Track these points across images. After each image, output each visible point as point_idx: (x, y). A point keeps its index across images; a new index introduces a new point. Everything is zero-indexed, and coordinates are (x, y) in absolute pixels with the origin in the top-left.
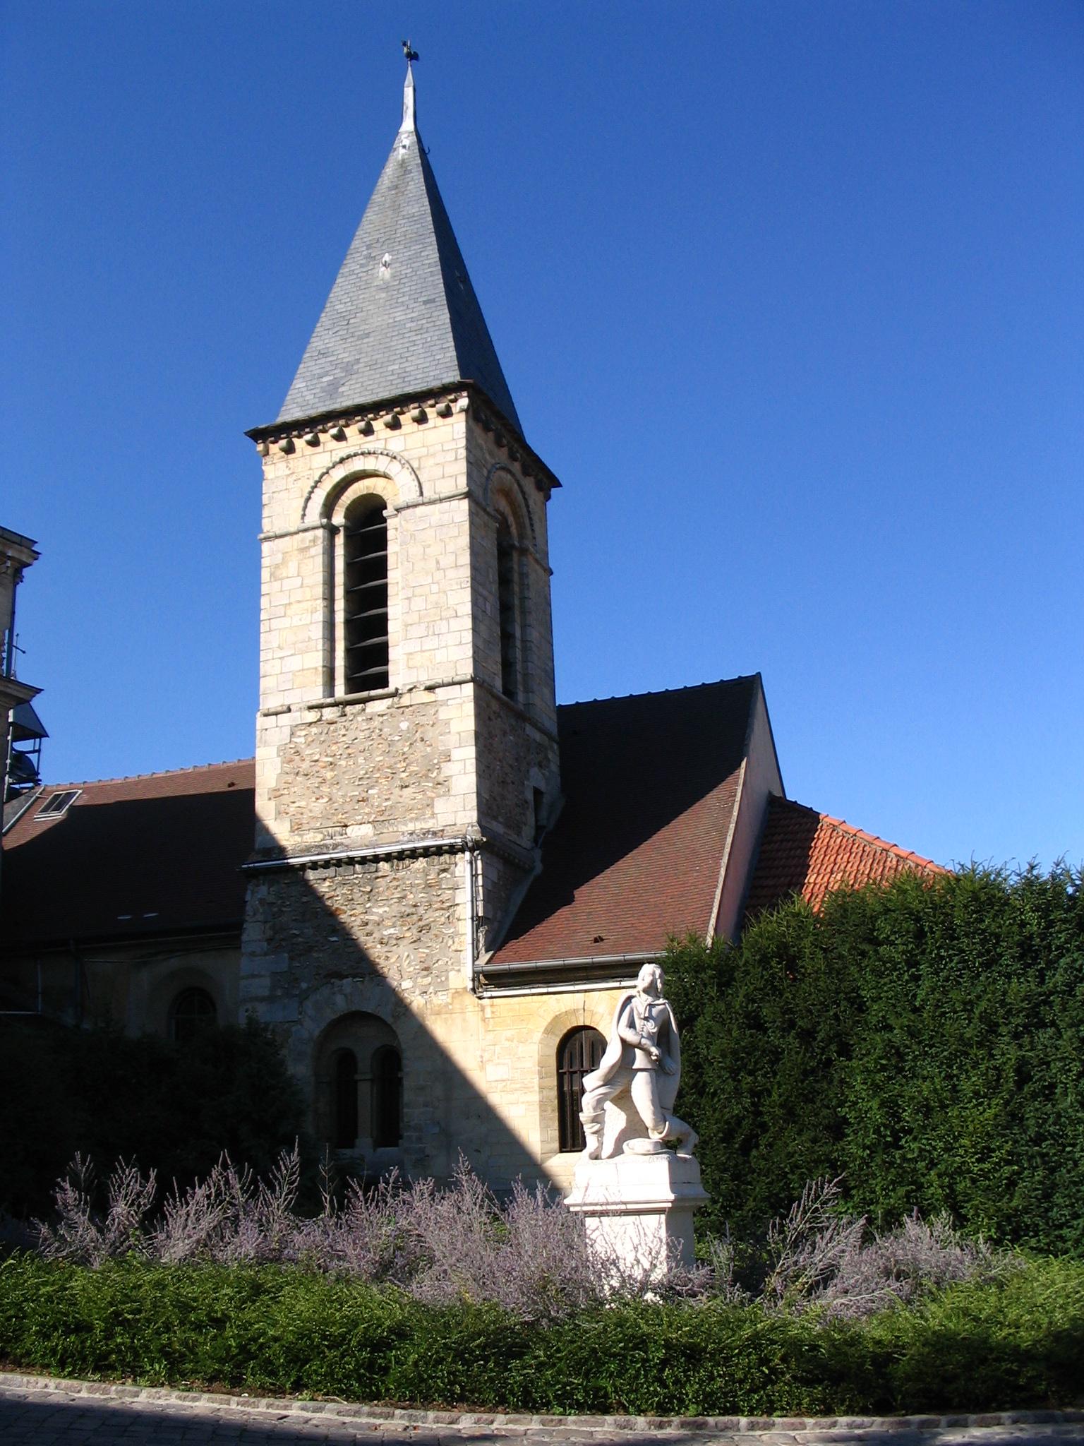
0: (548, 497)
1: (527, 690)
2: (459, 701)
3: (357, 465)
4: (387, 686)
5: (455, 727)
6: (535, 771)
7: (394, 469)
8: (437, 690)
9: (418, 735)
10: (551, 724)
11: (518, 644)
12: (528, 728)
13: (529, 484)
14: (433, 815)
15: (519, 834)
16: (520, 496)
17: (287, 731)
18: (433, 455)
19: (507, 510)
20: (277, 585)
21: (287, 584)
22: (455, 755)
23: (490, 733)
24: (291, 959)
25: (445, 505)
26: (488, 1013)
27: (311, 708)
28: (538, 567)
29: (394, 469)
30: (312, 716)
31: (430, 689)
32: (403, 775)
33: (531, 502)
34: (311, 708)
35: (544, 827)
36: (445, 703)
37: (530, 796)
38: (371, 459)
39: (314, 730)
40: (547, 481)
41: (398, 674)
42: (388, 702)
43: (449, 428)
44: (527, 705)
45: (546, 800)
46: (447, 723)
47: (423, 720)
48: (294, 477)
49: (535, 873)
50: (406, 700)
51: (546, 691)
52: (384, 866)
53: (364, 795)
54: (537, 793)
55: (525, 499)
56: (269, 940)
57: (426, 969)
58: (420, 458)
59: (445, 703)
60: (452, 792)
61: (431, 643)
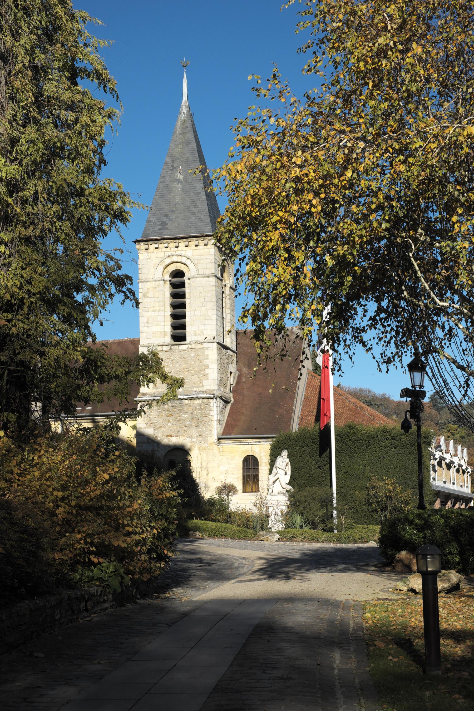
3: (175, 259)
5: (210, 357)
14: (203, 386)
20: (145, 300)
22: (210, 366)
24: (155, 430)
25: (207, 279)
26: (221, 450)
36: (207, 348)
38: (180, 257)
42: (187, 346)
46: (207, 355)
49: (231, 402)
52: (186, 402)
54: (231, 373)
56: (146, 424)
57: (201, 435)
60: (210, 378)
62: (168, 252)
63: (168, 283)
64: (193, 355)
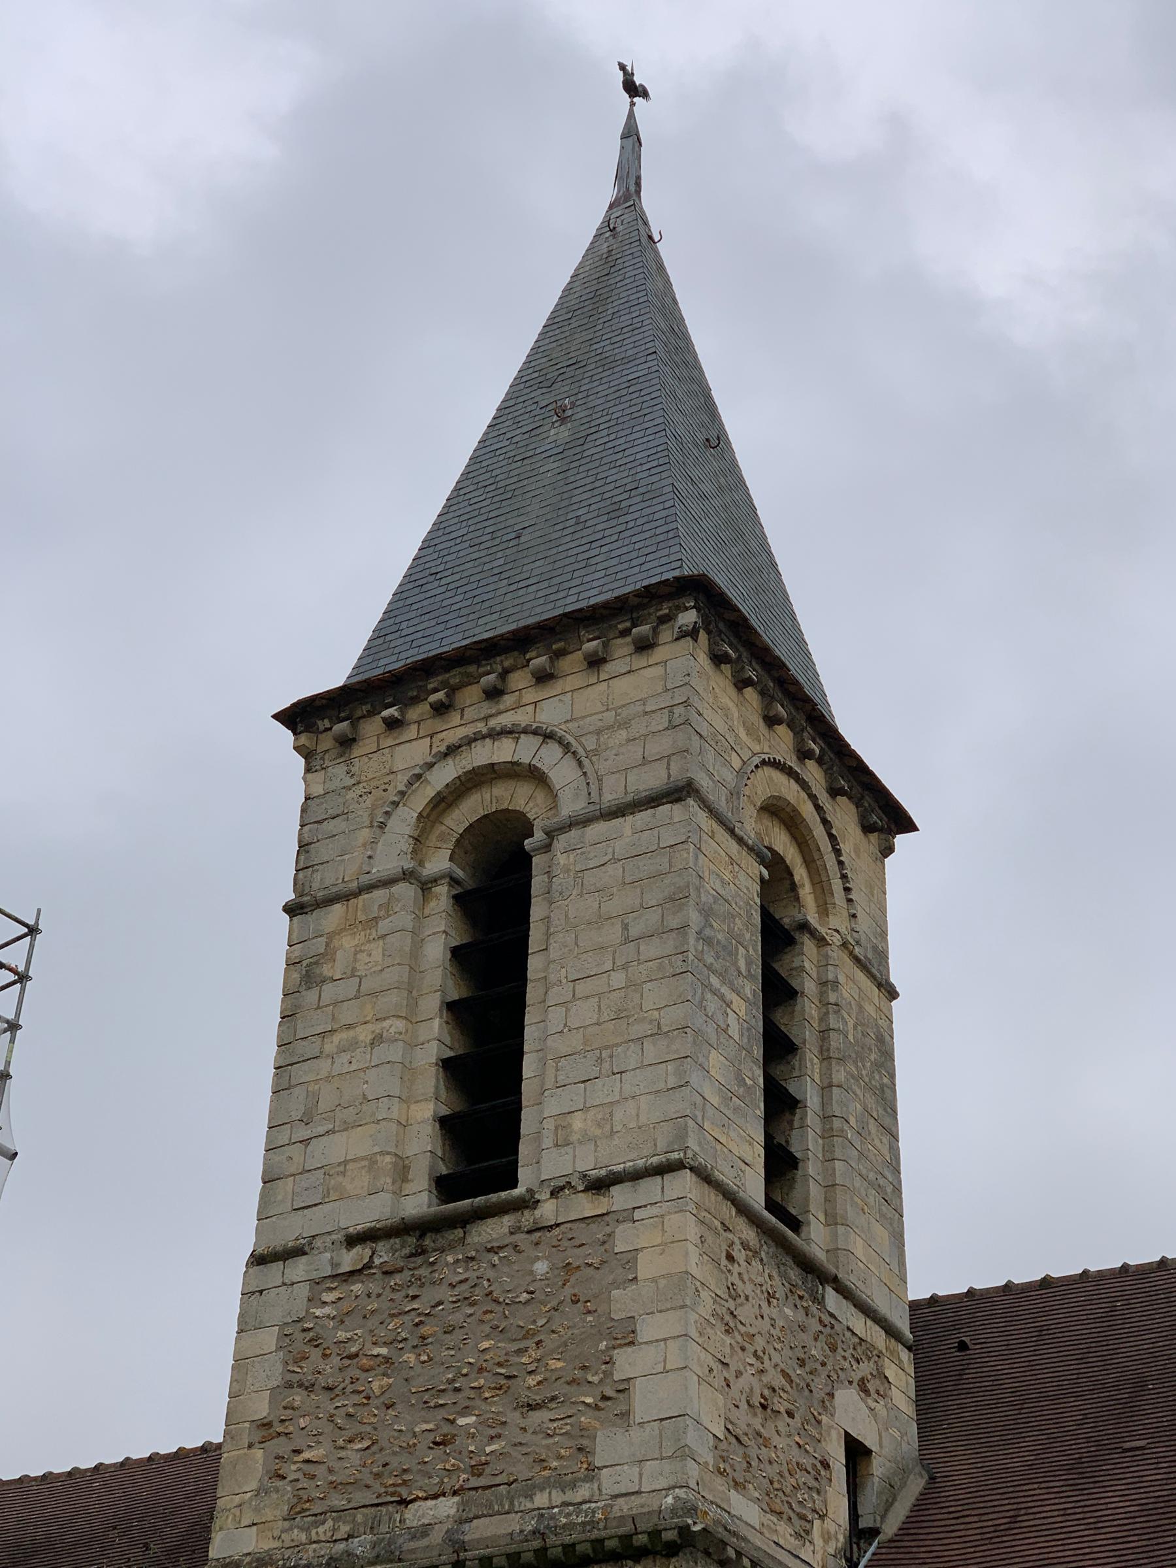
0: (888, 850)
1: (832, 1220)
2: (655, 1210)
3: (483, 755)
4: (514, 1184)
6: (846, 1397)
7: (549, 758)
8: (615, 1190)
9: (568, 1291)
10: (903, 1324)
11: (812, 1119)
12: (832, 1298)
13: (844, 816)
15: (803, 1535)
16: (819, 832)
17: (303, 1291)
18: (625, 724)
19: (782, 842)
21: (329, 992)
23: (731, 1289)
27: (352, 1241)
28: (860, 976)
29: (549, 758)
30: (349, 1259)
31: (599, 1186)
32: (531, 1381)
33: (845, 847)
34: (352, 1241)
35: (874, 1532)
37: (837, 1454)
39: (357, 1288)
40: (888, 819)
41: (541, 1160)
42: (507, 1221)
43: (658, 671)
44: (832, 1252)
45: (878, 1468)
46: (630, 1259)
47: (575, 1257)
48: (359, 790)
50: (547, 1210)
51: (881, 1233)
53: (446, 1429)
54: (856, 1452)
55: (832, 837)
58: (599, 732)
59: (628, 1216)
60: (638, 1415)
61: (602, 1092)
62: (454, 729)
63: (443, 891)
64: (541, 1267)
